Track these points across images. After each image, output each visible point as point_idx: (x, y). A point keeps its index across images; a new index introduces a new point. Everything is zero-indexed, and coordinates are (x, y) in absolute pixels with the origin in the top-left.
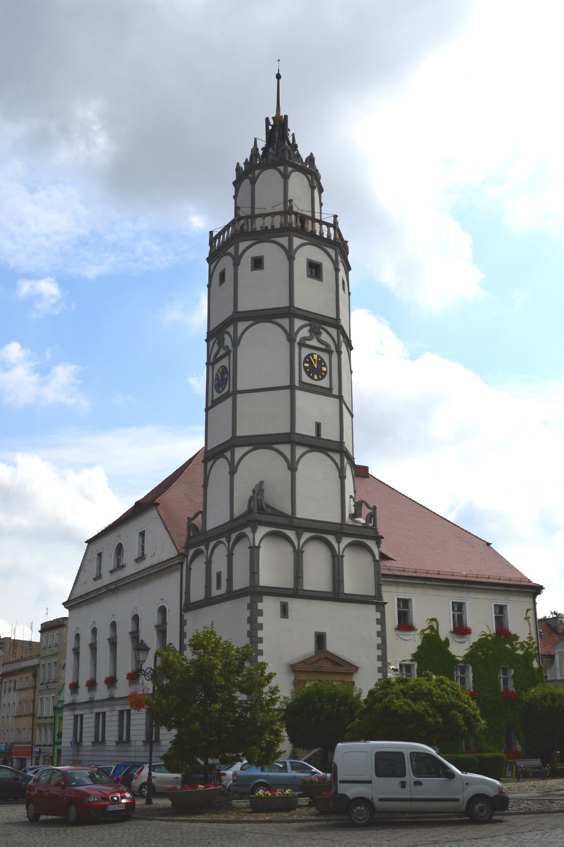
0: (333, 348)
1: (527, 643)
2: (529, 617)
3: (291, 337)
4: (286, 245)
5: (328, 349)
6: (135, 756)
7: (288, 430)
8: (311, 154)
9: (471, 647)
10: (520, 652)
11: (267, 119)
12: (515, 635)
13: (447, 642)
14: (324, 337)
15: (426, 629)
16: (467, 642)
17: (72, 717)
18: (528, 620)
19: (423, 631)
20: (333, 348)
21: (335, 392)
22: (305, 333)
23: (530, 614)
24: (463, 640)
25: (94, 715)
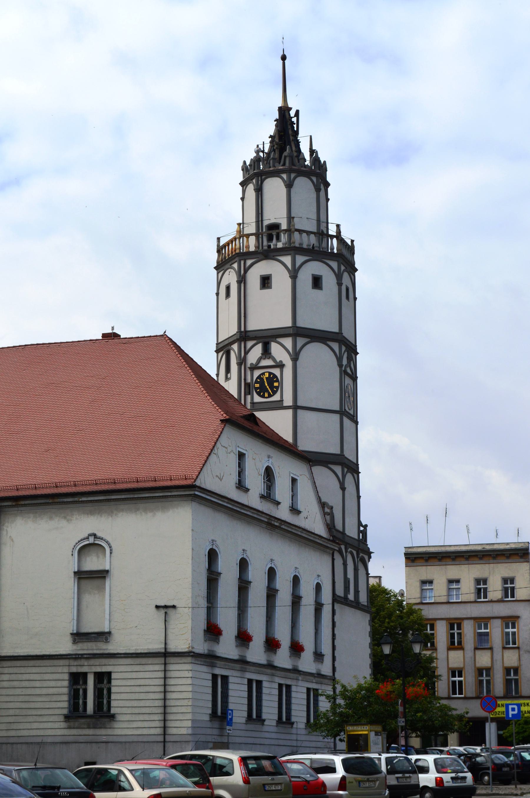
6: (297, 740)
17: (210, 677)
25: (246, 682)
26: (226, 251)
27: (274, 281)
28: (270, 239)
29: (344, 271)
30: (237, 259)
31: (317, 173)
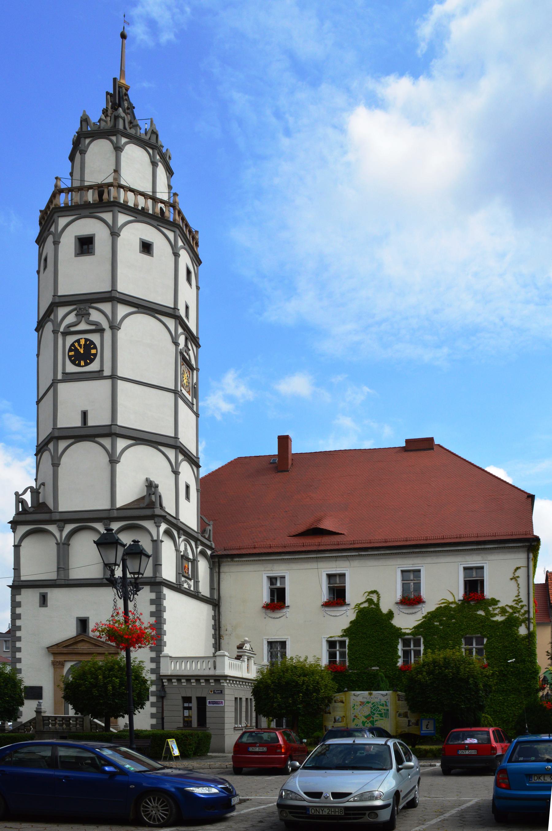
0: (105, 324)
1: (511, 607)
2: (518, 577)
4: (110, 222)
5: (99, 328)
7: (108, 422)
8: (84, 111)
9: (423, 617)
10: (499, 618)
12: (493, 599)
13: (390, 614)
14: (95, 316)
15: (362, 603)
16: (419, 613)
18: (516, 580)
19: (358, 605)
20: (105, 324)
21: (107, 372)
23: (522, 573)
24: (414, 611)
29: (182, 334)
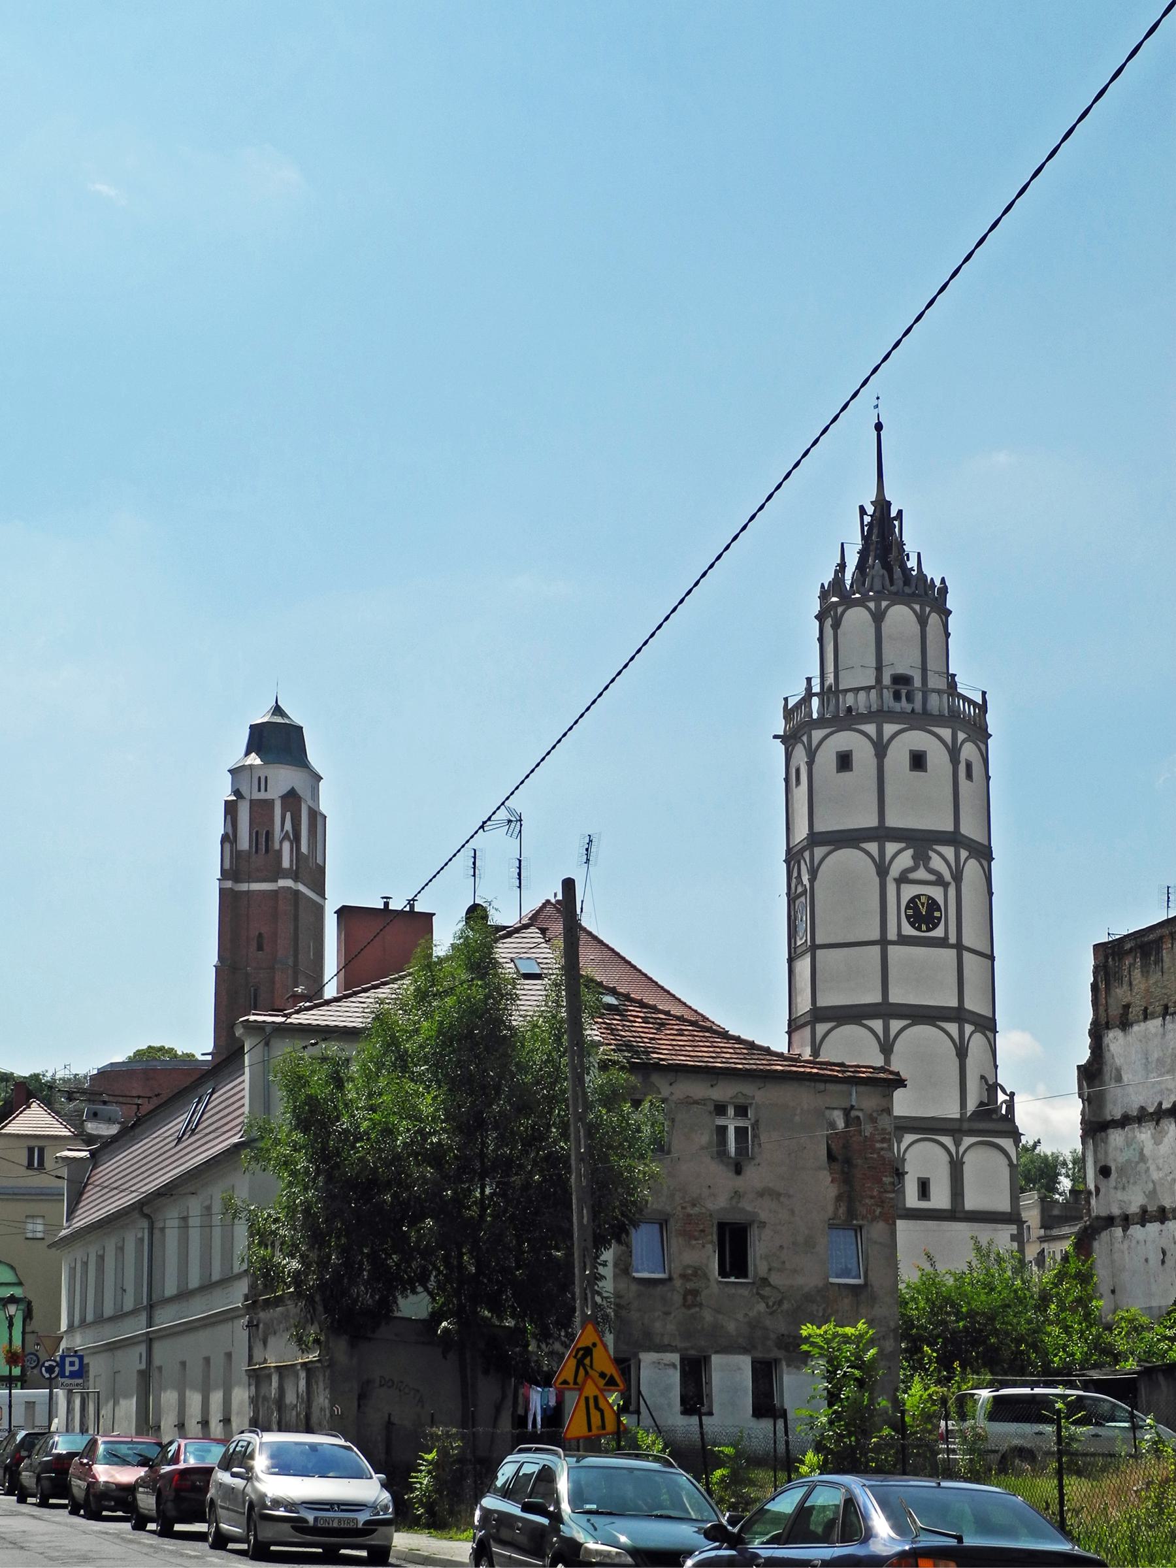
0: (947, 877)
3: (882, 870)
11: (862, 509)
14: (936, 863)
20: (947, 877)
21: (953, 940)
22: (905, 860)
26: (798, 718)
27: (856, 759)
28: (897, 696)
30: (806, 729)
31: (930, 599)
